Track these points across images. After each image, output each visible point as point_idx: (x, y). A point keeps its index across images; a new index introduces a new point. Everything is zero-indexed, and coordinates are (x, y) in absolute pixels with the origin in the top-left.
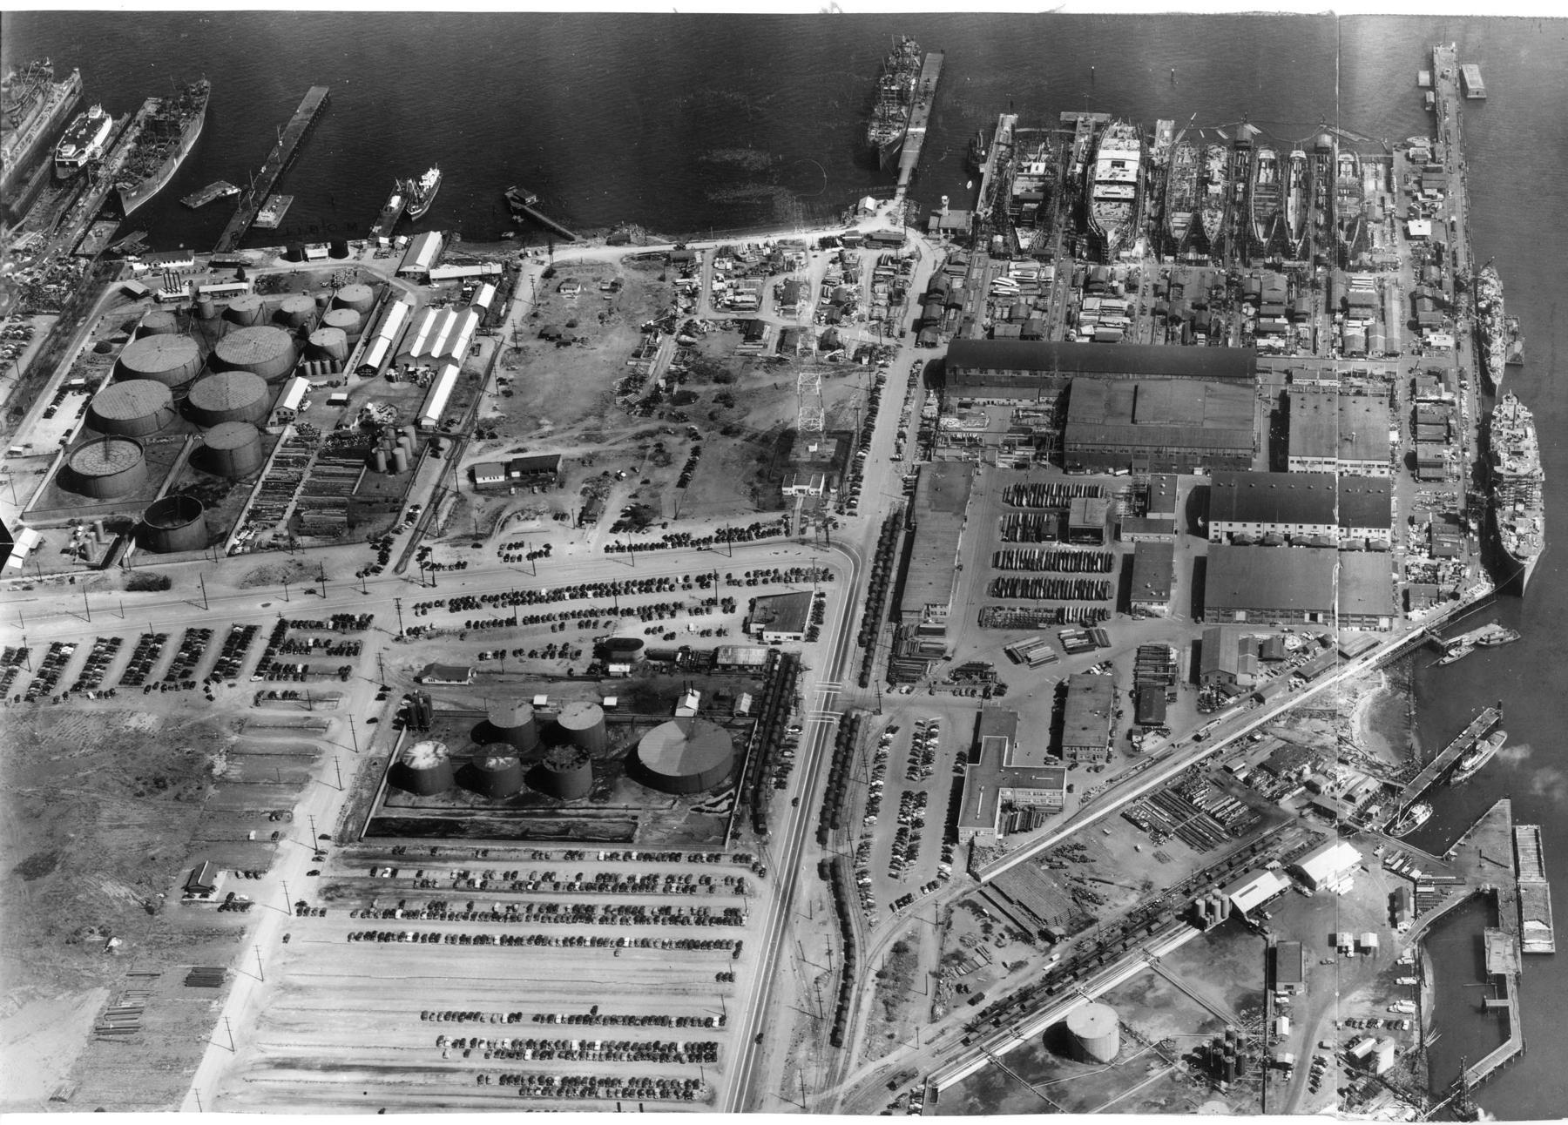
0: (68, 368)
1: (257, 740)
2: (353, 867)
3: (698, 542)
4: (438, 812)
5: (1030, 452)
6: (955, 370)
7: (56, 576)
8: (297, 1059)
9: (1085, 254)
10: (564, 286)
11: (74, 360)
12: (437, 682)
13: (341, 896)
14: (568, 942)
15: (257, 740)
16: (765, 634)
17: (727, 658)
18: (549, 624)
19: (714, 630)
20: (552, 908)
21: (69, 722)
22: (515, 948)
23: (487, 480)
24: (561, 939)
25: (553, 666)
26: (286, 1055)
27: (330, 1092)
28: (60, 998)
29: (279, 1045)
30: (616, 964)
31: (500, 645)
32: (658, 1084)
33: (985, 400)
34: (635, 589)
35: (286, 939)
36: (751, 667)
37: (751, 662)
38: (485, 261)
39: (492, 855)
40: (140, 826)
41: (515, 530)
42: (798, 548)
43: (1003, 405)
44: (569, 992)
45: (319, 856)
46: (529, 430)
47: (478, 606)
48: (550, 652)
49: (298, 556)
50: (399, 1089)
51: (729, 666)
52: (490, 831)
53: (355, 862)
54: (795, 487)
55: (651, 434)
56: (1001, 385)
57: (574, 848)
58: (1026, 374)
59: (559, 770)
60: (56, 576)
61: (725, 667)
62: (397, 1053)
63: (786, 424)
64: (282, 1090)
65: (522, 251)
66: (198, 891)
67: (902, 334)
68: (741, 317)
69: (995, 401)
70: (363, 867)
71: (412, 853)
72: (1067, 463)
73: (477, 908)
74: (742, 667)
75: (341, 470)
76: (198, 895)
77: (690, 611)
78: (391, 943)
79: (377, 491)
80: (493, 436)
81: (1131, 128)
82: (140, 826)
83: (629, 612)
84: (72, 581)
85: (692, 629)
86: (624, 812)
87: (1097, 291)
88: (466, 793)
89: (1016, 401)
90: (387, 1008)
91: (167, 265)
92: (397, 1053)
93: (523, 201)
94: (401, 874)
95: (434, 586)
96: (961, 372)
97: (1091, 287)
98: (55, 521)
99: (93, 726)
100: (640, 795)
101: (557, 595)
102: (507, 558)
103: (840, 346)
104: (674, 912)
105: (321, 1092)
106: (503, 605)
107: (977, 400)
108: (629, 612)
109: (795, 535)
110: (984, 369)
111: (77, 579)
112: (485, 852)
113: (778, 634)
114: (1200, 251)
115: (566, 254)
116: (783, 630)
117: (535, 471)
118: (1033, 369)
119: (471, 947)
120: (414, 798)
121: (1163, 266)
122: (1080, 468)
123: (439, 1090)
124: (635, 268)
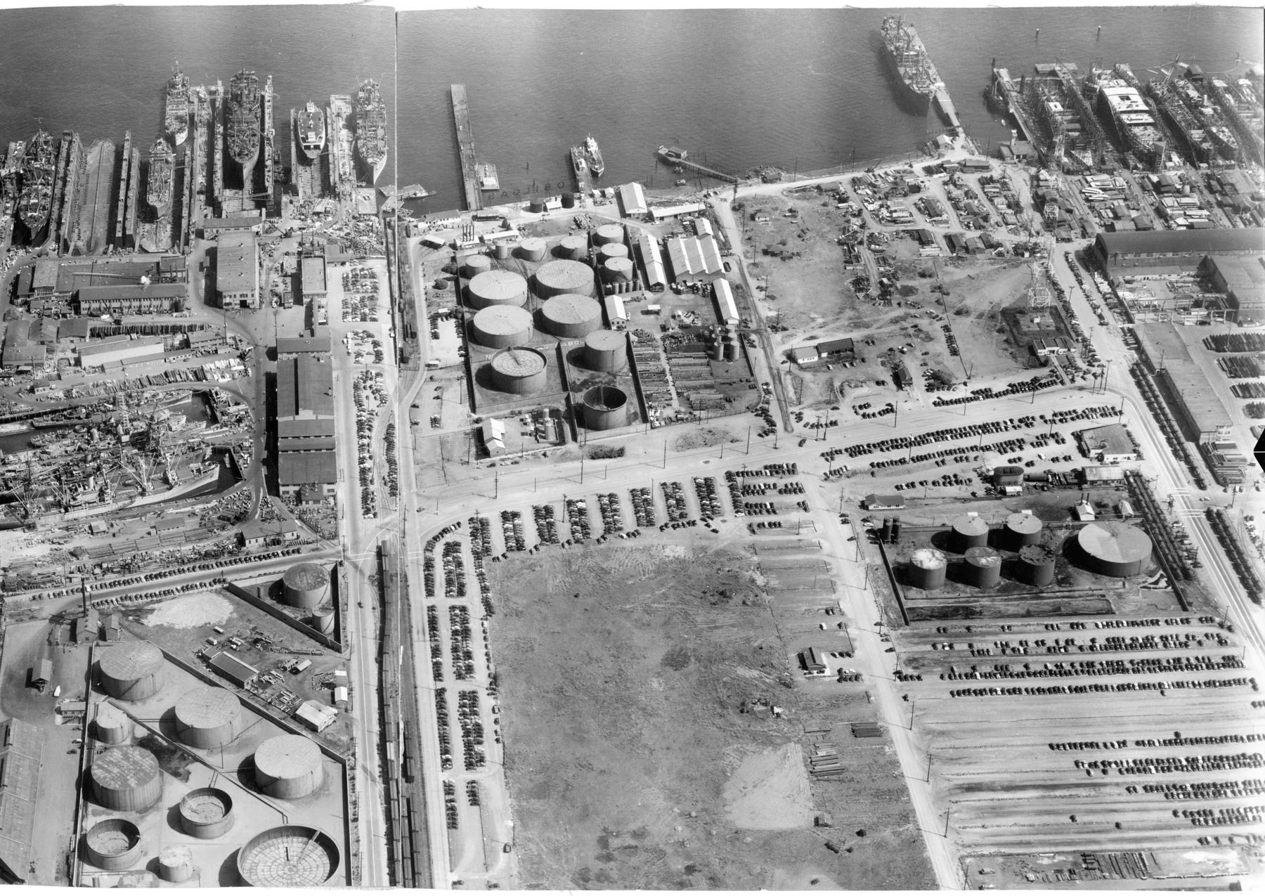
0: (424, 304)
1: (773, 558)
2: (916, 644)
3: (996, 395)
4: (950, 601)
5: (1203, 312)
6: (1116, 255)
7: (530, 452)
8: (980, 784)
9: (1140, 166)
10: (759, 215)
11: (424, 297)
12: (880, 508)
13: (923, 665)
14: (1121, 688)
15: (773, 558)
16: (1106, 456)
17: (1095, 475)
18: (933, 461)
19: (1061, 457)
20: (1091, 665)
21: (621, 555)
22: (1083, 695)
23: (806, 361)
24: (1115, 686)
25: (954, 490)
26: (966, 782)
27: (1020, 805)
28: (765, 752)
29: (958, 775)
30: (1163, 701)
31: (910, 479)
32: (764, 871)
33: (1142, 277)
34: (948, 436)
35: (905, 698)
36: (1113, 481)
37: (1113, 478)
38: (681, 202)
39: (1014, 629)
40: (733, 626)
41: (854, 395)
42: (1077, 394)
43: (1156, 280)
44: (1148, 723)
45: (885, 639)
46: (807, 323)
47: (766, 467)
48: (947, 480)
49: (704, 425)
50: (1069, 800)
51: (1096, 482)
52: (1000, 612)
53: (916, 640)
54: (1048, 349)
55: (904, 318)
56: (1151, 265)
57: (1075, 620)
58: (1170, 255)
59: (1037, 563)
60: (530, 452)
61: (1093, 482)
62: (1050, 775)
63: (999, 304)
64: (986, 807)
65: (704, 192)
66: (815, 669)
67: (1038, 233)
68: (909, 228)
69: (1150, 277)
70: (925, 643)
71: (953, 631)
72: (1240, 318)
73: (1033, 668)
74: (1106, 482)
75: (692, 361)
76: (815, 672)
77: (1032, 444)
78: (985, 696)
79: (725, 374)
80: (785, 329)
81: (1109, 72)
82: (733, 626)
83: (987, 448)
84: (545, 455)
85: (1043, 457)
86: (1090, 592)
87: (1167, 192)
88: (960, 586)
89: (1166, 276)
90: (1019, 743)
91: (443, 222)
92: (1050, 775)
93: (678, 156)
94: (957, 647)
95: (824, 439)
96: (1120, 257)
97: (1163, 189)
98: (502, 413)
99: (641, 558)
100: (1094, 580)
101: (922, 440)
102: (864, 416)
103: (1000, 245)
104: (1184, 662)
105: (1015, 806)
106: (888, 449)
107: (1136, 277)
108: (987, 448)
109: (1068, 384)
110: (1138, 254)
111: (548, 453)
112: (1009, 627)
113: (1116, 456)
114: (1226, 158)
115: (744, 192)
116: (1118, 453)
117: (838, 352)
118: (1175, 251)
119: (1048, 696)
120: (924, 592)
121: (1200, 172)
122: (1251, 322)
123: (1098, 800)
124: (798, 198)
